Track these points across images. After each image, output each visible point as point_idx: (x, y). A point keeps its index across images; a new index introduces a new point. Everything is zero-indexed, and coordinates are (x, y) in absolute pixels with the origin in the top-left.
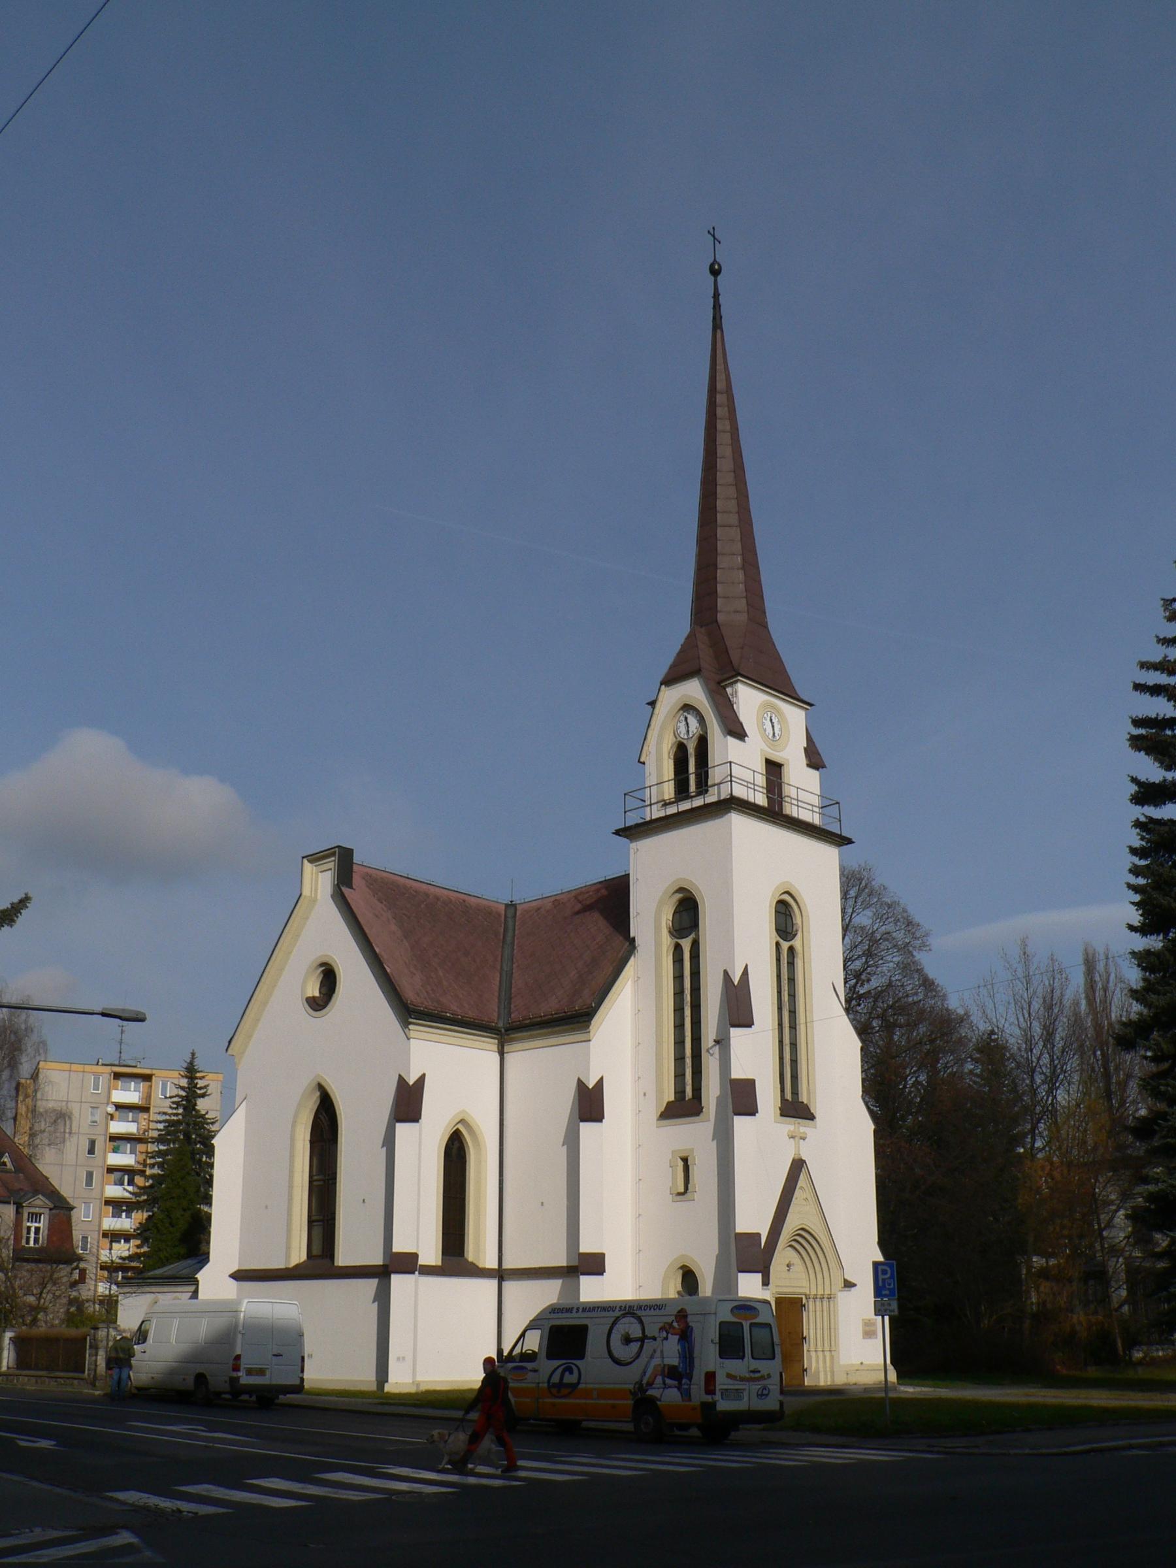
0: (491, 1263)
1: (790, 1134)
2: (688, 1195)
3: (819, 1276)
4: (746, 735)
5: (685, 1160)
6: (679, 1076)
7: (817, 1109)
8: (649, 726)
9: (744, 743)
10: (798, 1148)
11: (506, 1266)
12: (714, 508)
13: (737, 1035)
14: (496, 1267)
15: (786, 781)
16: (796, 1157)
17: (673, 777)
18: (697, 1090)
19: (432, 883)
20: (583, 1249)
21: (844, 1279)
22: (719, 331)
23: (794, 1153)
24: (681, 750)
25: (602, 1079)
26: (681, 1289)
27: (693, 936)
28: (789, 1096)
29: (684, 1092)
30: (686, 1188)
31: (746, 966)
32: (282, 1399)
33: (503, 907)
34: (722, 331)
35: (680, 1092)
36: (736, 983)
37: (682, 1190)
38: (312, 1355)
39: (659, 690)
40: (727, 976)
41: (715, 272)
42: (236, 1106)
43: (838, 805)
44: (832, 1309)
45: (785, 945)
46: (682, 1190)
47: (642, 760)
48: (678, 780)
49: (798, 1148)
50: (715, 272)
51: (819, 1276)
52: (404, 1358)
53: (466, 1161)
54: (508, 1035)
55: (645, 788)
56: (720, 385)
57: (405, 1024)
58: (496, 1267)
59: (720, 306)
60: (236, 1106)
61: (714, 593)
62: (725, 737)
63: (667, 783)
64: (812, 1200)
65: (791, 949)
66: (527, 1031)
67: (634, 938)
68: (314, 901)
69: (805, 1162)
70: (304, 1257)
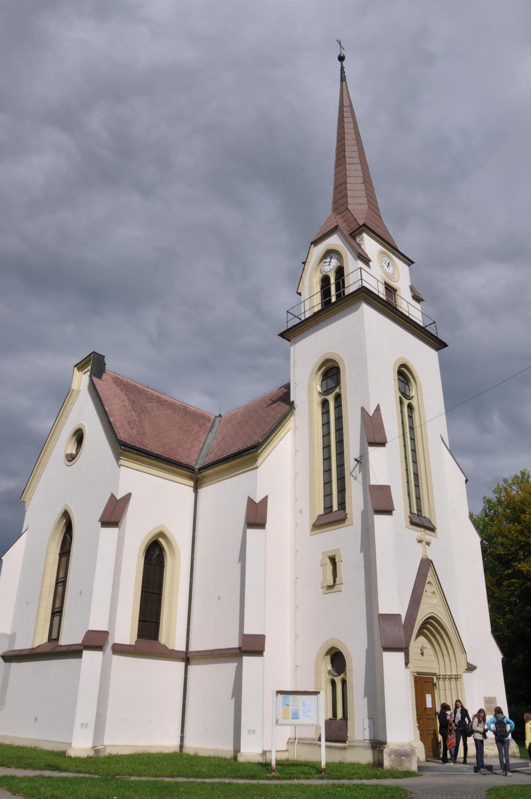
0: (179, 645)
1: (419, 539)
2: (336, 588)
3: (453, 662)
4: (361, 408)
5: (333, 560)
6: (328, 495)
7: (438, 523)
8: (303, 269)
9: (370, 269)
10: (425, 551)
11: (192, 649)
12: (344, 145)
13: (373, 452)
14: (183, 649)
15: (399, 305)
16: (424, 557)
17: (320, 290)
18: (342, 505)
19: (164, 394)
20: (247, 631)
21: (468, 663)
22: (344, 83)
23: (422, 554)
24: (325, 280)
25: (267, 497)
26: (331, 669)
27: (342, 676)
28: (415, 511)
29: (331, 507)
30: (335, 581)
31: (66, 515)
32: (435, 687)
33: (214, 417)
34: (346, 83)
35: (328, 508)
36: (371, 415)
37: (331, 583)
38: (37, 718)
39: (310, 247)
40: (363, 411)
41: (341, 59)
42: (23, 533)
43: (434, 324)
44: (459, 688)
45: (406, 402)
46: (331, 583)
47: (299, 291)
48: (324, 291)
49: (425, 551)
50: (341, 59)
51: (453, 662)
52: (87, 724)
53: (164, 566)
54: (200, 473)
55: (301, 303)
56: (346, 103)
57: (118, 457)
58: (183, 649)
59: (345, 72)
60: (23, 533)
61: (344, 138)
62: (356, 261)
63: (316, 306)
64: (438, 593)
65: (410, 407)
66: (213, 468)
67: (293, 402)
68: (79, 392)
69: (432, 562)
70: (45, 640)
